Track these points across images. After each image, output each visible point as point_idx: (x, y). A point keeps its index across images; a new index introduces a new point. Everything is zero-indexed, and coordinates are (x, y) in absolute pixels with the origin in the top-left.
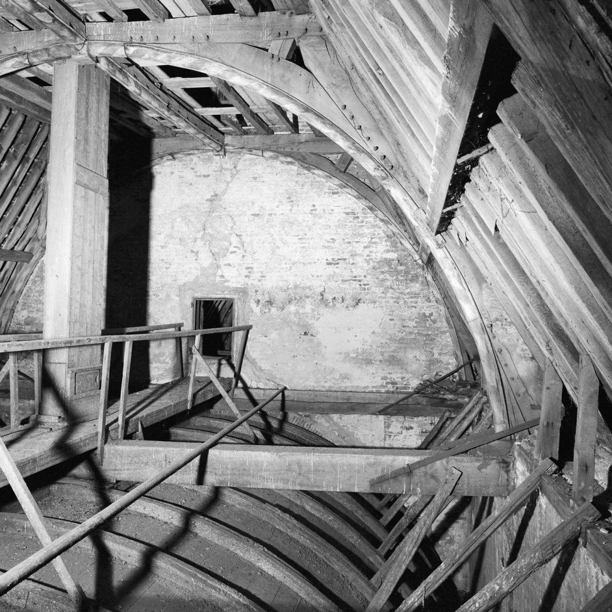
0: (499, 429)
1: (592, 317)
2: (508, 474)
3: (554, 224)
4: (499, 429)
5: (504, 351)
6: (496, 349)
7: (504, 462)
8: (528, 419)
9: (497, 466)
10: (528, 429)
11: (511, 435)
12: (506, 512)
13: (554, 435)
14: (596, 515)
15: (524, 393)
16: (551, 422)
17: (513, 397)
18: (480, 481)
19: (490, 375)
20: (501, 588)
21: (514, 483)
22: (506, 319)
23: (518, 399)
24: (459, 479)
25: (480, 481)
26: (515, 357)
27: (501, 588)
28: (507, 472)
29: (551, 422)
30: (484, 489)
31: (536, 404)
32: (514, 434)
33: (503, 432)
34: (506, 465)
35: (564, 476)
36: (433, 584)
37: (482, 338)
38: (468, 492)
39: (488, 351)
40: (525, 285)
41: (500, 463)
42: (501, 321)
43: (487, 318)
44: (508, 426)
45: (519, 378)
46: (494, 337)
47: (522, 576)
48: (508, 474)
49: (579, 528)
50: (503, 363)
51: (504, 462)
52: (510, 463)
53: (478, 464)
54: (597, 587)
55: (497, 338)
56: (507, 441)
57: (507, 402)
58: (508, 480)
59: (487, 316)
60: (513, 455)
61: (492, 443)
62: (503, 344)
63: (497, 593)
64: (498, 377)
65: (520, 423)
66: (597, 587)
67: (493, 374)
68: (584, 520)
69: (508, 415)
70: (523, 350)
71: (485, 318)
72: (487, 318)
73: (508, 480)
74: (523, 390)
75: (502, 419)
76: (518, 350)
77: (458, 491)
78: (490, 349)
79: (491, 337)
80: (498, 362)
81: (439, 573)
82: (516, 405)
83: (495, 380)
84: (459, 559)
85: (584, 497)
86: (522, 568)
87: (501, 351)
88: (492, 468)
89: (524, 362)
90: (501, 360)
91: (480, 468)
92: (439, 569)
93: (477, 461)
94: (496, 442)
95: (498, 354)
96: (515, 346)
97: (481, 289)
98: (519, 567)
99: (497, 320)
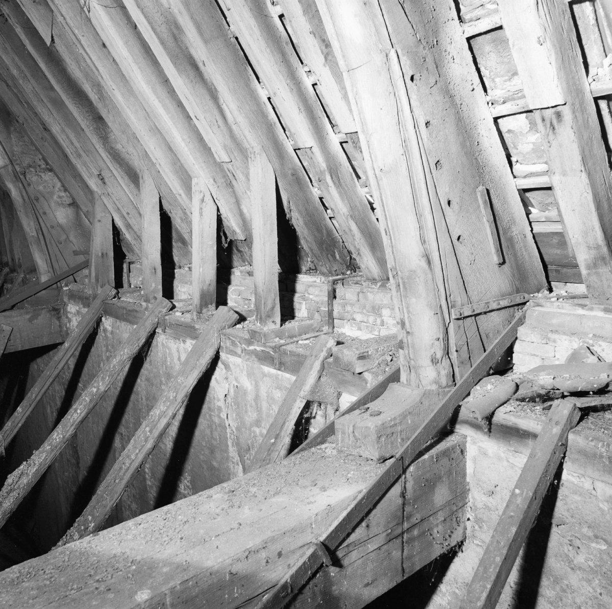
0: (44, 279)
1: (167, 116)
2: (59, 321)
3: (143, 13)
4: (44, 279)
5: (42, 199)
6: (33, 197)
7: (54, 309)
8: (72, 266)
9: (48, 315)
10: (72, 275)
11: (57, 283)
12: (75, 342)
13: (109, 264)
14: (168, 305)
15: (66, 241)
16: (105, 252)
17: (54, 245)
18: (32, 333)
19: (29, 224)
20: (98, 389)
21: (66, 327)
22: (39, 166)
23: (60, 246)
24: (10, 335)
25: (32, 333)
26: (53, 204)
27: (98, 389)
28: (59, 318)
29: (105, 252)
30: (38, 339)
31: (78, 250)
32: (60, 281)
33: (49, 280)
34: (57, 312)
35: (122, 299)
36: (12, 430)
37: (15, 186)
38: (22, 346)
39: (24, 200)
40: (80, 106)
41: (50, 311)
42: (35, 167)
43: (19, 164)
44: (53, 273)
45: (60, 226)
46: (29, 185)
47: (115, 373)
48: (59, 321)
49: (157, 320)
50: (41, 211)
51: (54, 309)
52: (60, 309)
53: (28, 317)
54: (179, 359)
55: (32, 186)
56: (54, 289)
57: (50, 251)
58: (60, 326)
59: (18, 162)
60: (62, 300)
61: (39, 294)
62: (38, 191)
63: (96, 395)
64: (38, 227)
65: (64, 270)
66: (179, 359)
67: (32, 223)
68: (160, 312)
69: (51, 263)
70: (60, 197)
71: (17, 164)
72: (19, 164)
73: (60, 326)
74: (64, 237)
75: (46, 269)
76: (55, 197)
77: (11, 347)
78: (26, 198)
79: (26, 185)
80: (36, 211)
81: (16, 417)
82: (59, 253)
83: (34, 229)
84: (36, 397)
85: (156, 295)
86: (114, 366)
87: (37, 200)
88: (44, 318)
89: (62, 209)
90: (38, 208)
91: (30, 320)
92: (16, 414)
93: (27, 313)
94: (43, 292)
95: (35, 201)
96: (52, 194)
97: (9, 133)
98: (112, 367)
99: (30, 166)
